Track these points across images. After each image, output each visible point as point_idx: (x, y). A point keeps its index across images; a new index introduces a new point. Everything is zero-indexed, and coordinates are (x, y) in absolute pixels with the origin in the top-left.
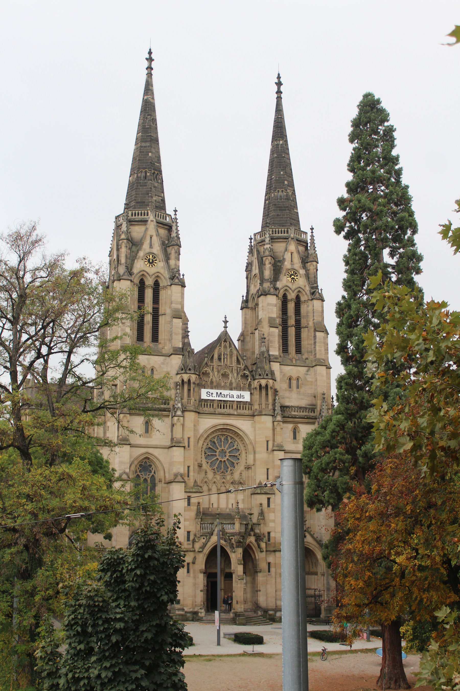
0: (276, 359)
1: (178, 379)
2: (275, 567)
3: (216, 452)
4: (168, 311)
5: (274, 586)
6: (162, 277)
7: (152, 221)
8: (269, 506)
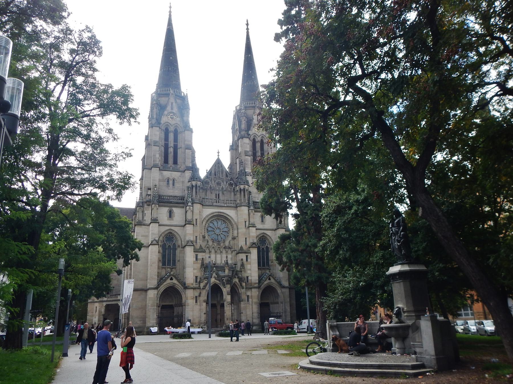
1: (189, 184)
4: (183, 146)
7: (172, 94)
8: (247, 260)
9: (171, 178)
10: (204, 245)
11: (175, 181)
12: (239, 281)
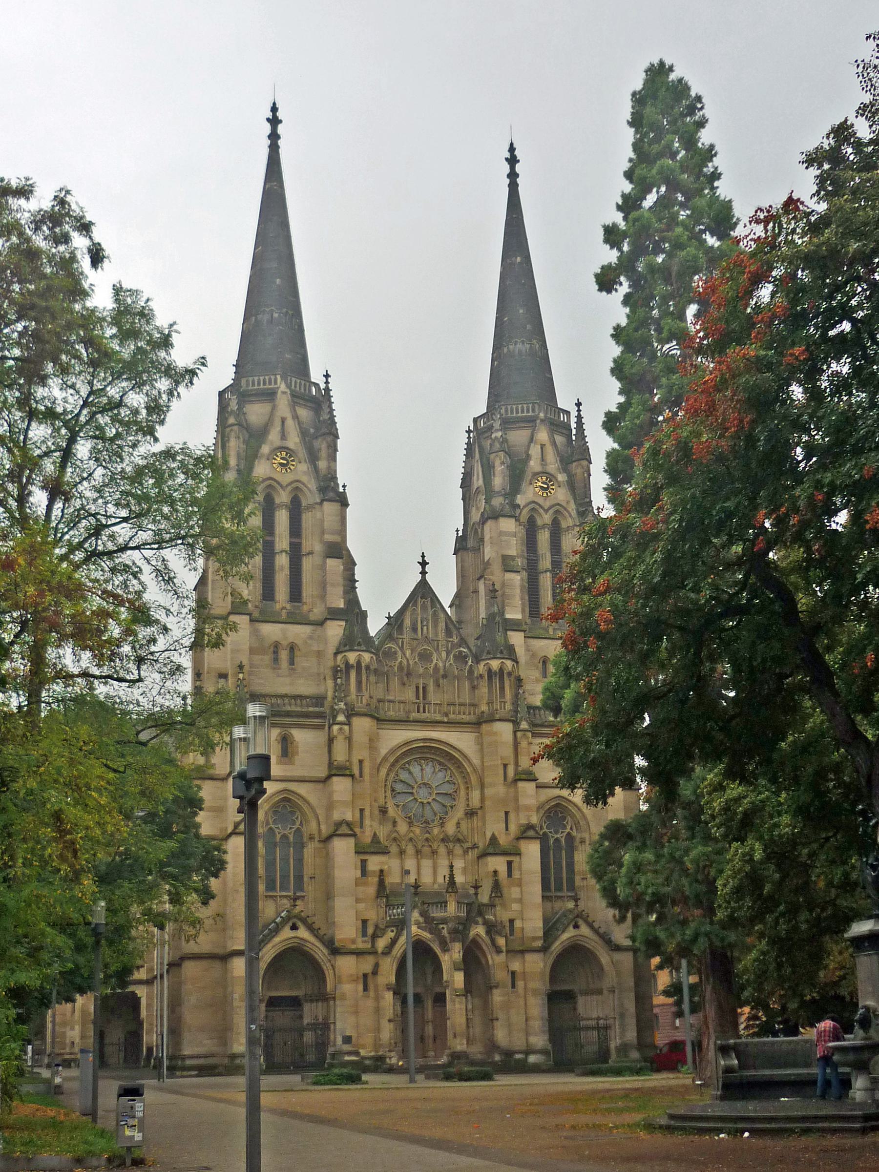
0: (515, 626)
2: (524, 980)
3: (413, 788)
4: (318, 548)
5: (523, 1011)
6: (305, 489)
7: (284, 393)
9: (285, 643)
10: (383, 833)
11: (297, 653)
12: (488, 933)
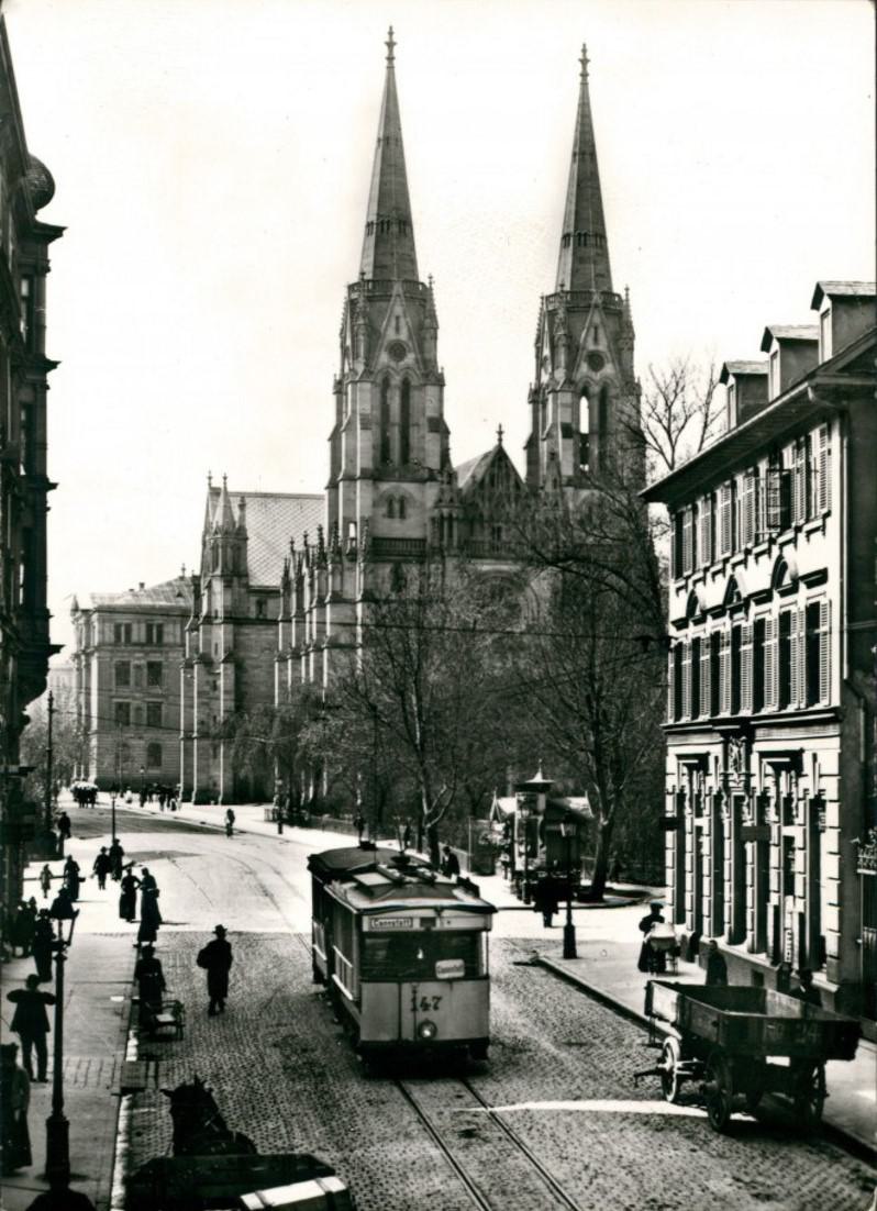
1: (436, 513)
11: (407, 506)
